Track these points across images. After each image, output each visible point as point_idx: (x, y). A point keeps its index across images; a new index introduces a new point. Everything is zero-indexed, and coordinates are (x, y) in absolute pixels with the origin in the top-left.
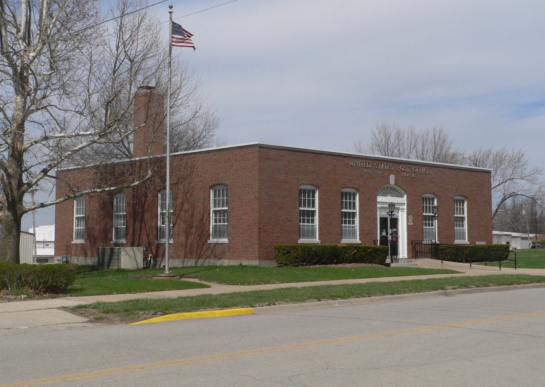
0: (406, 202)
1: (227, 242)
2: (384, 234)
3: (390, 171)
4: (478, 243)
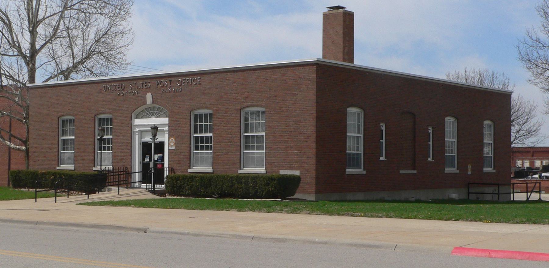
2: (147, 160)
3: (148, 90)
4: (282, 172)
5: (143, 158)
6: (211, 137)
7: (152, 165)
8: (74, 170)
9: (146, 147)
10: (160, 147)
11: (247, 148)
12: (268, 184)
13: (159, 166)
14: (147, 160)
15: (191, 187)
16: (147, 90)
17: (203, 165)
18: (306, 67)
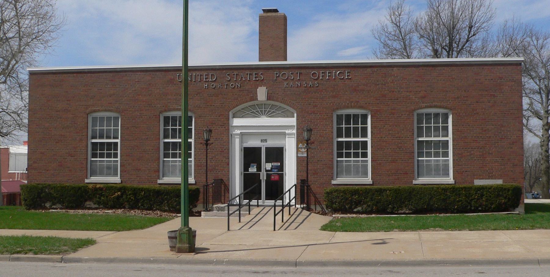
0: (295, 124)
1: (371, 183)
2: (253, 170)
3: (261, 83)
4: (478, 182)
5: (246, 167)
6: (180, 142)
7: (263, 176)
8: (372, 185)
9: (251, 155)
10: (277, 154)
11: (94, 155)
12: (498, 196)
13: (274, 178)
14: (253, 170)
15: (377, 202)
16: (258, 83)
17: (358, 174)
18: (508, 67)
